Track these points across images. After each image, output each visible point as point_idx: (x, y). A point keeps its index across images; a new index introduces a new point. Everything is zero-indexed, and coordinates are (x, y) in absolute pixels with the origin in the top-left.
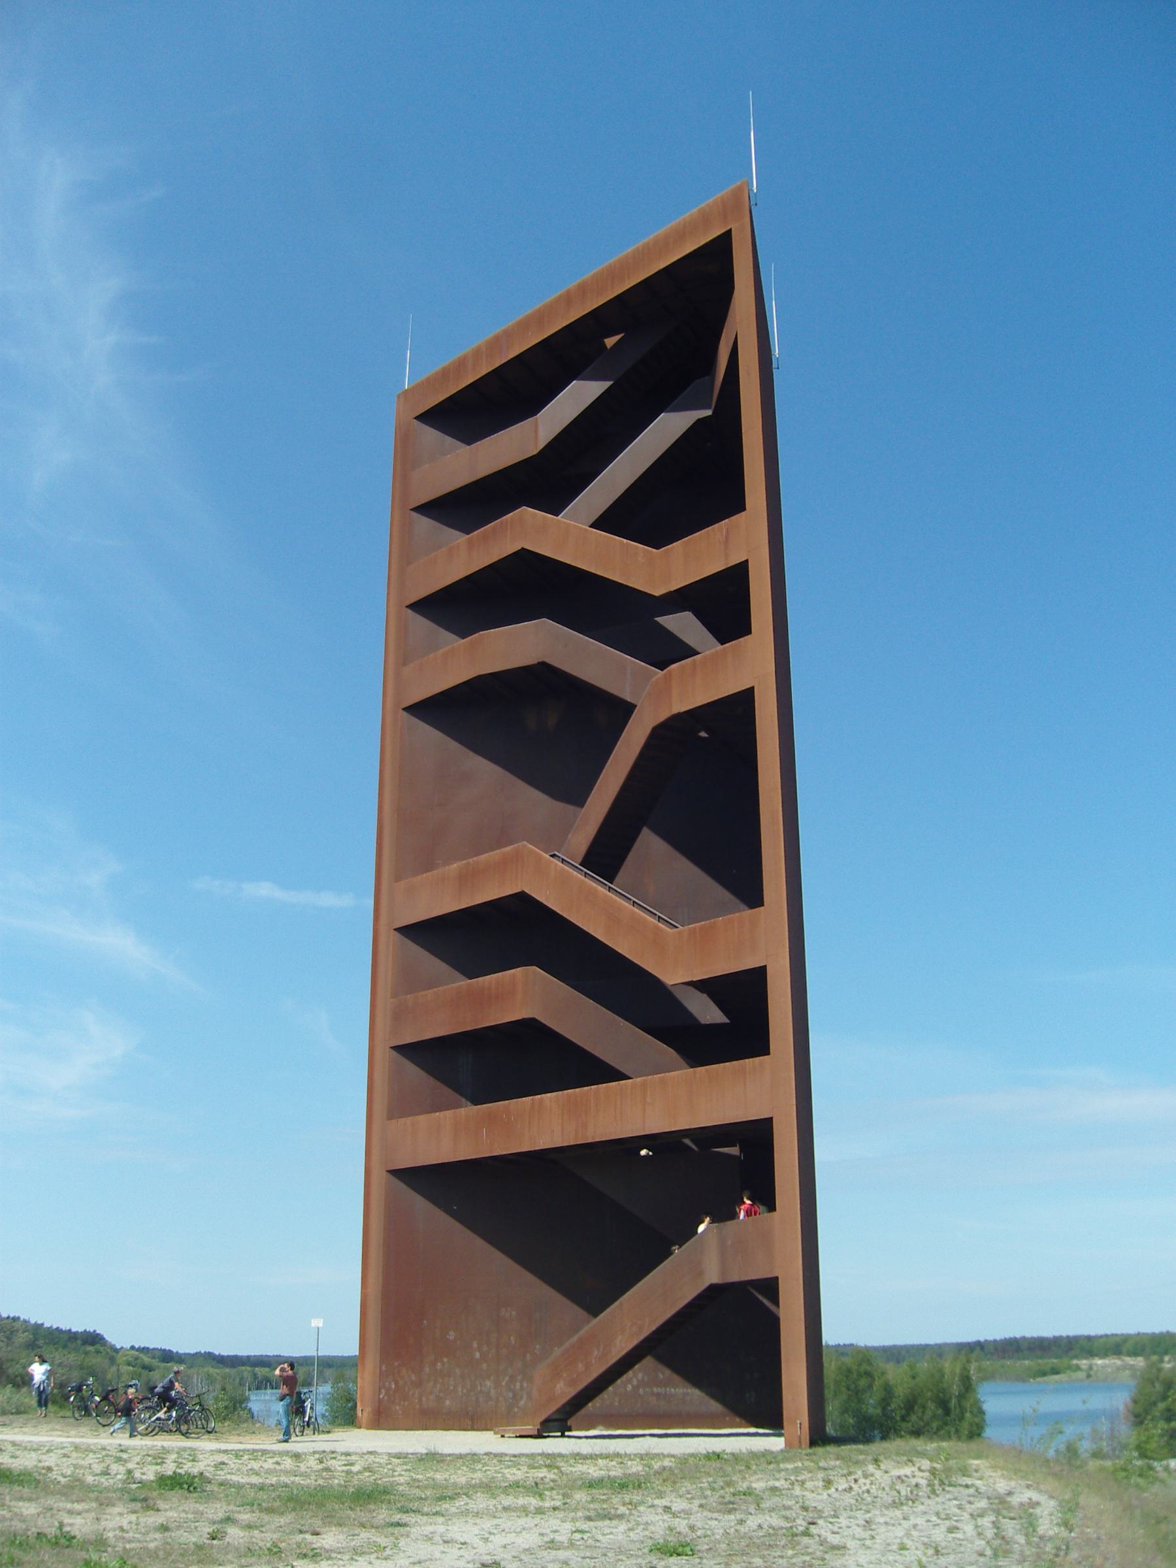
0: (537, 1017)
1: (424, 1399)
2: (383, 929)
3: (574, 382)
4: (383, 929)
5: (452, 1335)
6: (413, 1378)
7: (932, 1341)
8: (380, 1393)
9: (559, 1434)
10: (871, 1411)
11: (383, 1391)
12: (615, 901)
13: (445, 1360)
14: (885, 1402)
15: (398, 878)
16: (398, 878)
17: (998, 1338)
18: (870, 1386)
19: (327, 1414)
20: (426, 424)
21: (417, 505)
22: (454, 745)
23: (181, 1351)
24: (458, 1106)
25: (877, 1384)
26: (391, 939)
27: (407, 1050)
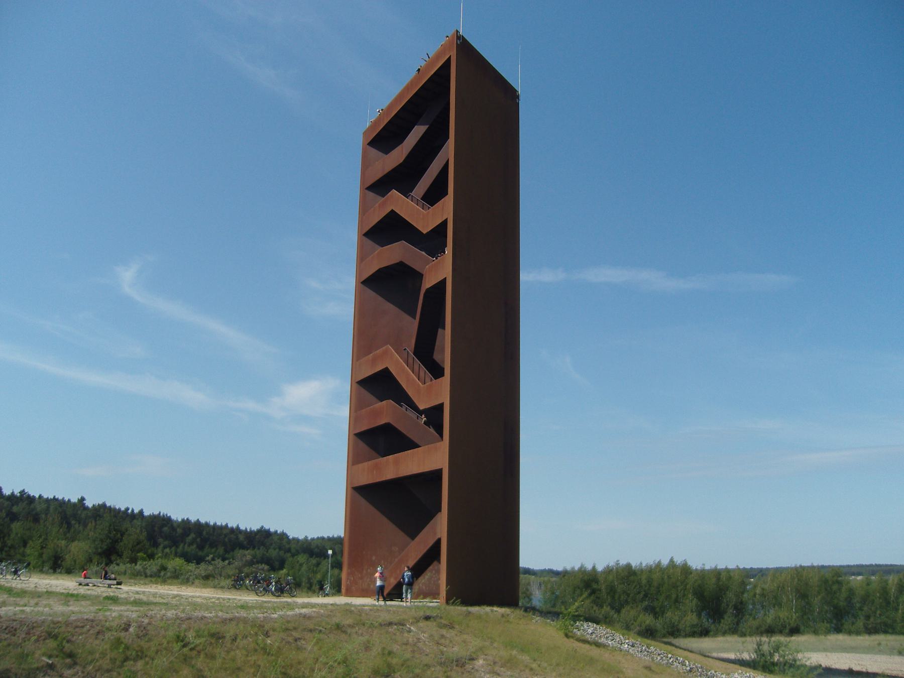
0: (391, 423)
1: (363, 585)
2: (353, 383)
3: (416, 126)
4: (353, 383)
5: (374, 558)
6: (360, 576)
7: (756, 566)
8: (347, 581)
9: (400, 600)
10: (841, 604)
11: (349, 581)
12: (408, 371)
13: (371, 568)
14: (849, 599)
15: (357, 360)
16: (357, 360)
17: (695, 564)
18: (840, 589)
19: (541, 600)
20: (373, 147)
21: (368, 186)
22: (380, 298)
23: (535, 568)
24: (379, 458)
25: (843, 589)
26: (355, 385)
27: (357, 435)
